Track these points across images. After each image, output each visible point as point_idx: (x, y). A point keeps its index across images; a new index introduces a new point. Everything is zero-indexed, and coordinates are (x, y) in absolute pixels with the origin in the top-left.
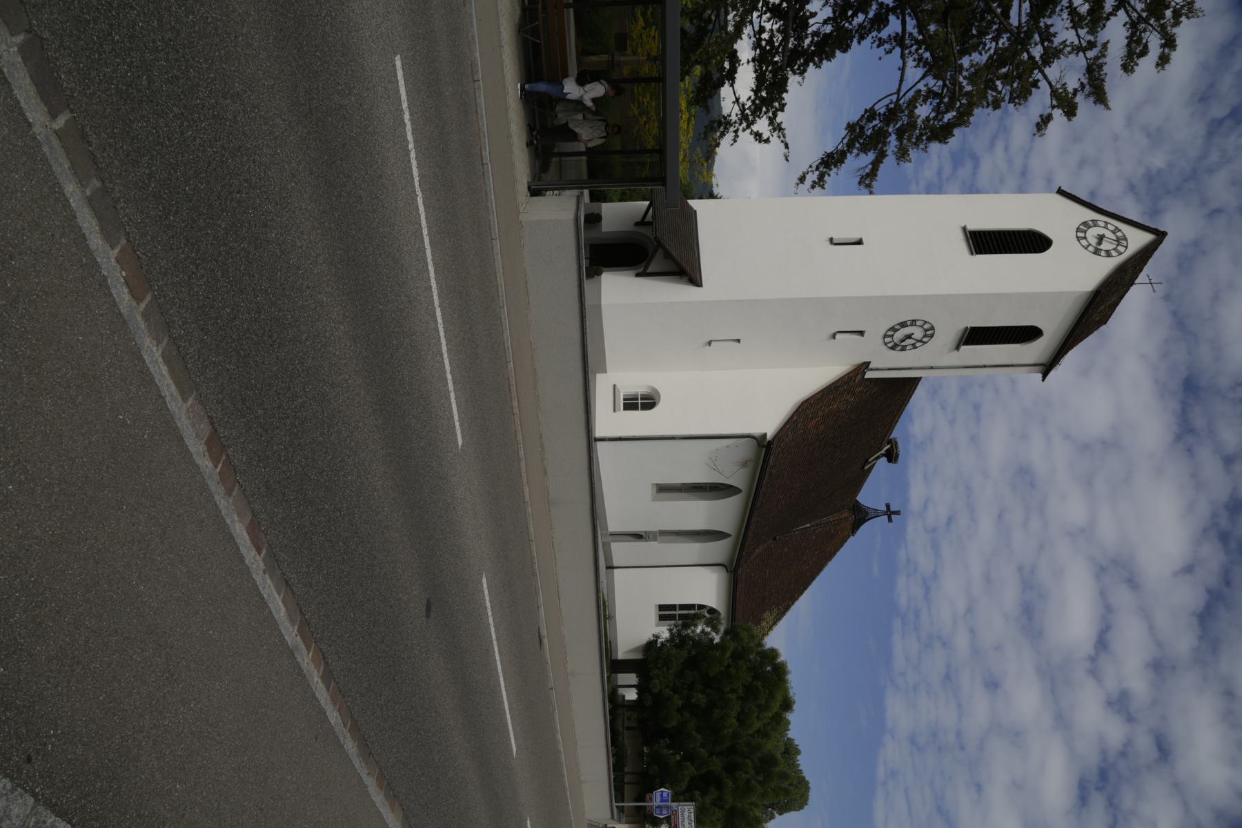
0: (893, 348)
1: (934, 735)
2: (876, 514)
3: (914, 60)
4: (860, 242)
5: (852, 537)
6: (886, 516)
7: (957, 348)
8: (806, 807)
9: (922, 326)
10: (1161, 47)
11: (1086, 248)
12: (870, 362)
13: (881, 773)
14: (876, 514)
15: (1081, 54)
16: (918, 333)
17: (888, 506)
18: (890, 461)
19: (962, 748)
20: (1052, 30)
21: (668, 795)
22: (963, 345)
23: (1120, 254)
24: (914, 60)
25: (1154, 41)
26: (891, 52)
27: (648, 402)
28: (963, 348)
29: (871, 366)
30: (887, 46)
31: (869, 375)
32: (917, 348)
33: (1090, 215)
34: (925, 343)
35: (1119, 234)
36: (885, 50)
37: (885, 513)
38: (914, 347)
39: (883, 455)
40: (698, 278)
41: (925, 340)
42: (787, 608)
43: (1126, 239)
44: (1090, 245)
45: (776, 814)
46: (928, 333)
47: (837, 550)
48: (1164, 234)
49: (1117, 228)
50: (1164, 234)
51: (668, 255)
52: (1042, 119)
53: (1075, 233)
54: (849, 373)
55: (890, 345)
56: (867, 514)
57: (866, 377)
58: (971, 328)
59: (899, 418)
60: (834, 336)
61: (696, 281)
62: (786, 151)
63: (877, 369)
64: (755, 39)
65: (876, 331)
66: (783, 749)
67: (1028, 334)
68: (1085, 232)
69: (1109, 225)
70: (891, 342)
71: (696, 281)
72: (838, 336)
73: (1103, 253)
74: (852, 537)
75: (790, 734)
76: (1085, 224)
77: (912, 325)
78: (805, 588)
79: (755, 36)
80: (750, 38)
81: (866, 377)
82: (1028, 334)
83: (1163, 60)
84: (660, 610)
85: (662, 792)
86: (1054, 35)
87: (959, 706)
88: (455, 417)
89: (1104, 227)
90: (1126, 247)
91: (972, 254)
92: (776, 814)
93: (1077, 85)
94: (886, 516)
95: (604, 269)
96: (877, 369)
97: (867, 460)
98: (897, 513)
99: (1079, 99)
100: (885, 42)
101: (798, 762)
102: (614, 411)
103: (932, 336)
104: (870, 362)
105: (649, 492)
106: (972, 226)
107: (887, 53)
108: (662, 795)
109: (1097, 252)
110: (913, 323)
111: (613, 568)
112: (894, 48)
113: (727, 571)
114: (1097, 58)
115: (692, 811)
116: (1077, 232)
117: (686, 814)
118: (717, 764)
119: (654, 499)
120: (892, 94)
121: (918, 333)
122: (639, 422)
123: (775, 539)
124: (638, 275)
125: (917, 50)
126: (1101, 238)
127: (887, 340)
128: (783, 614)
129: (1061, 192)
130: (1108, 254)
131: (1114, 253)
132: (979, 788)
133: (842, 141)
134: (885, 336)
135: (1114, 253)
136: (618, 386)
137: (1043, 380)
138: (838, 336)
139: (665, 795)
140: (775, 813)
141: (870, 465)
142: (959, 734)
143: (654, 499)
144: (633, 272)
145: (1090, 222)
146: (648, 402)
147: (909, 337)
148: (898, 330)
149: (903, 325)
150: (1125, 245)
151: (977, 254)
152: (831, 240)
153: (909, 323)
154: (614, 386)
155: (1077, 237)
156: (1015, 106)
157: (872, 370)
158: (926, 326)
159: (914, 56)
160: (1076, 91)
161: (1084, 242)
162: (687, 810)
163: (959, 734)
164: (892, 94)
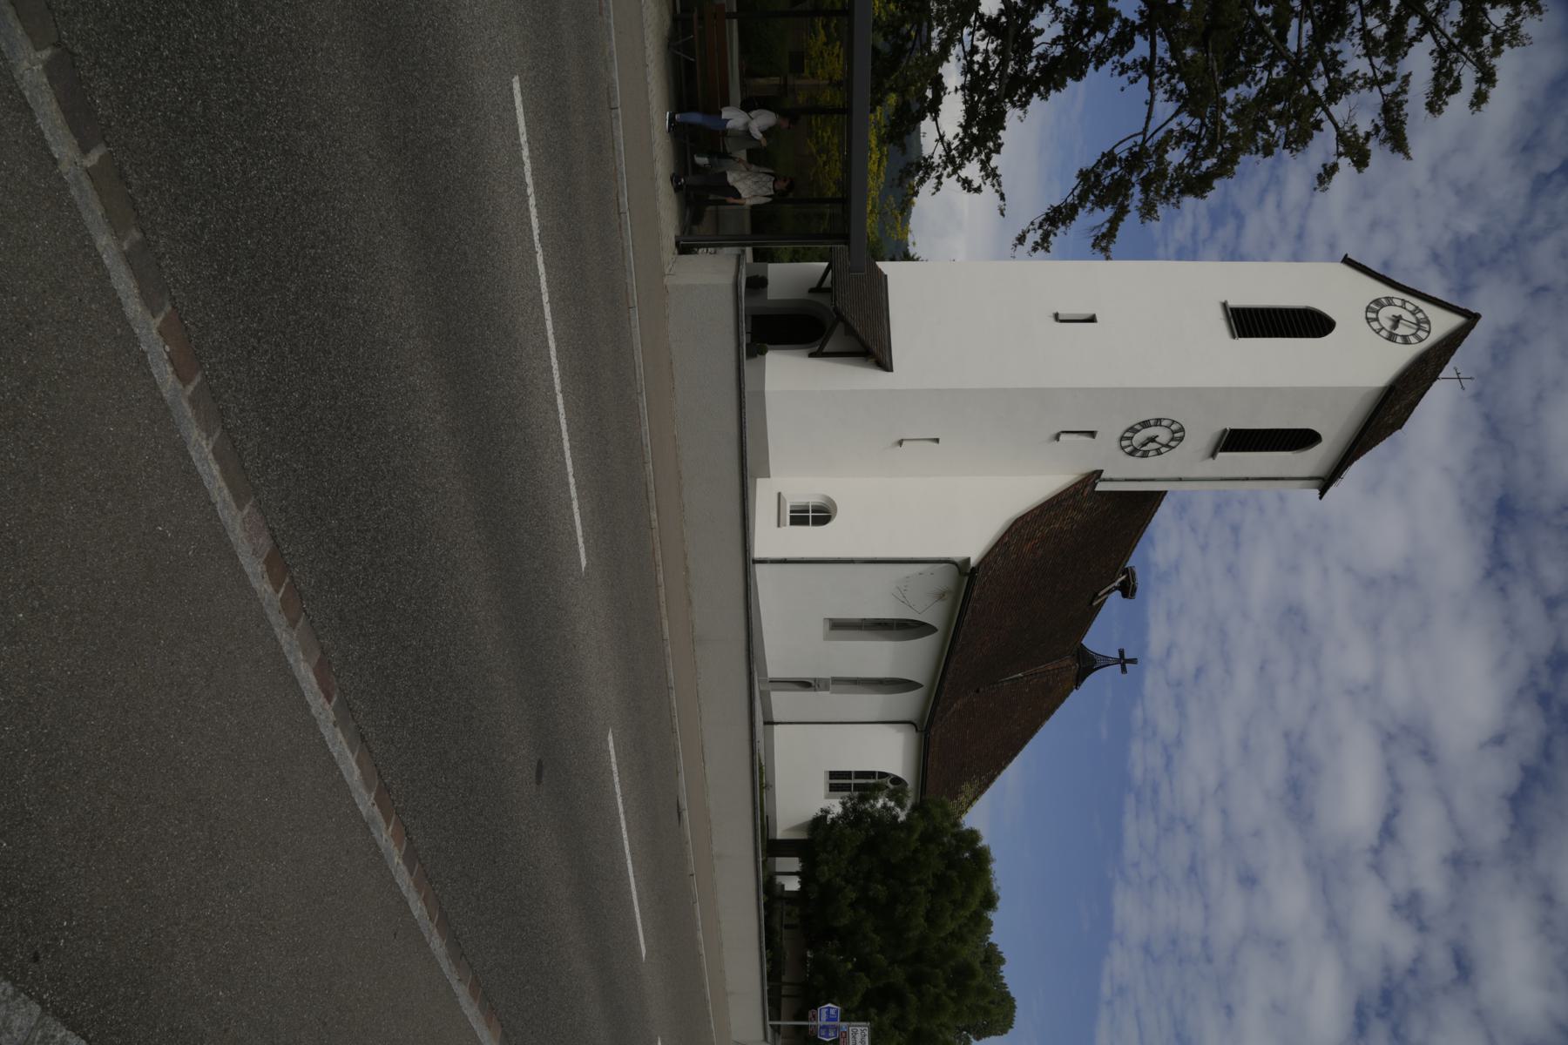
0: (1131, 454)
1: (1174, 942)
2: (1107, 662)
3: (1166, 92)
4: (1092, 319)
5: (1075, 690)
7: (1213, 455)
8: (1010, 1031)
10: (1477, 82)
11: (1378, 333)
12: (1102, 471)
13: (1106, 989)
14: (1107, 662)
15: (1376, 89)
16: (1163, 435)
17: (1121, 652)
18: (1125, 595)
19: (1209, 960)
20: (1340, 58)
21: (836, 1012)
22: (1221, 451)
23: (1421, 340)
24: (1166, 92)
25: (1468, 75)
26: (1136, 82)
27: (820, 515)
28: (1220, 455)
29: (1103, 476)
30: (1131, 74)
31: (1101, 487)
33: (1383, 291)
35: (1420, 316)
36: (1129, 78)
37: (1117, 661)
38: (1159, 453)
39: (1116, 588)
40: (888, 360)
41: (1173, 444)
42: (992, 779)
43: (1428, 322)
44: (1383, 328)
45: (972, 1040)
46: (1176, 435)
47: (1057, 706)
48: (1476, 317)
49: (1417, 308)
50: (1476, 317)
51: (850, 331)
52: (1325, 169)
54: (1076, 484)
55: (1128, 450)
57: (1097, 489)
58: (1231, 430)
60: (1057, 437)
61: (884, 364)
62: (1002, 203)
63: (1111, 480)
64: (965, 62)
65: (1110, 430)
66: (983, 958)
67: (1302, 439)
68: (1377, 312)
69: (1407, 304)
71: (884, 364)
72: (1063, 437)
73: (1399, 339)
74: (1075, 690)
75: (992, 938)
76: (1377, 301)
77: (1156, 425)
79: (965, 58)
80: (959, 60)
81: (1097, 489)
82: (1302, 439)
83: (1479, 99)
85: (829, 1008)
86: (1343, 64)
87: (1206, 907)
89: (1401, 307)
90: (1429, 332)
91: (1234, 337)
92: (972, 1040)
93: (1370, 128)
95: (768, 346)
96: (1111, 480)
97: (1097, 594)
98: (1133, 661)
99: (1372, 145)
100: (1129, 68)
101: (1001, 974)
102: (779, 526)
103: (1181, 439)
104: (1102, 471)
105: (820, 628)
106: (1233, 303)
107: (1131, 82)
108: (828, 1013)
109: (1391, 338)
110: (1158, 422)
111: (773, 723)
112: (1140, 77)
113: (917, 730)
114: (1396, 94)
115: (867, 1033)
116: (1367, 312)
117: (859, 1037)
118: (898, 975)
119: (827, 638)
120: (1136, 135)
121: (1163, 435)
122: (809, 541)
123: (978, 691)
124: (811, 355)
125: (1169, 80)
126: (1397, 320)
127: (1125, 443)
128: (987, 786)
129: (1347, 261)
130: (1406, 341)
131: (1413, 339)
132: (1229, 1010)
133: (1072, 192)
134: (1122, 438)
135: (1413, 339)
136: (783, 494)
137: (1321, 498)
138: (1063, 437)
139: (832, 1012)
140: (971, 1037)
141: (1099, 601)
142: (1205, 942)
143: (827, 638)
144: (805, 352)
145: (1383, 300)
146: (820, 515)
148: (1139, 431)
149: (1145, 424)
150: (1427, 329)
151: (1240, 337)
152: (1056, 316)
153: (1152, 422)
154: (779, 494)
155: (1367, 318)
156: (1291, 152)
157: (1104, 480)
158: (1174, 427)
159: (1165, 87)
160: (1368, 135)
161: (1375, 325)
162: (859, 1032)
163: (1205, 942)
164: (1136, 135)
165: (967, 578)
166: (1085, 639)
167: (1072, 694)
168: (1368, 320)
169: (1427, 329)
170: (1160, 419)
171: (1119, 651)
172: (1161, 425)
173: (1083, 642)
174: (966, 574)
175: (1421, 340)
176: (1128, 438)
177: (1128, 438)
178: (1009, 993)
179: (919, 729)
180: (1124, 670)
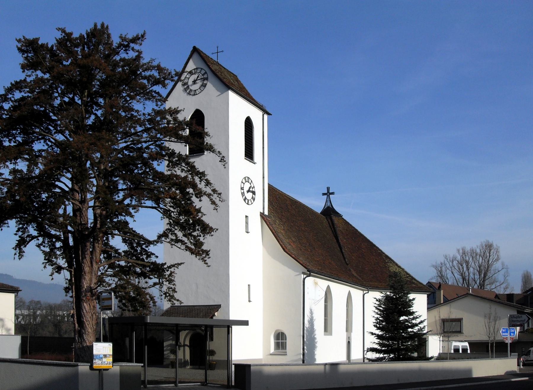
2: (329, 200)
5: (343, 217)
6: (327, 192)
9: (244, 184)
12: (260, 212)
14: (329, 200)
16: (247, 186)
17: (324, 194)
21: (504, 329)
29: (262, 212)
31: (266, 213)
32: (254, 186)
34: (252, 181)
37: (328, 197)
41: (250, 181)
42: (387, 257)
48: (194, 48)
50: (194, 48)
53: (191, 96)
55: (252, 201)
56: (328, 207)
57: (267, 214)
58: (245, 156)
59: (280, 191)
63: (264, 208)
70: (251, 201)
74: (343, 217)
76: (185, 90)
77: (243, 190)
78: (374, 246)
81: (267, 214)
84: (286, 352)
85: (502, 332)
88: (441, 386)
89: (189, 79)
90: (202, 69)
94: (327, 192)
96: (264, 208)
98: (328, 189)
103: (249, 178)
104: (260, 212)
108: (504, 332)
110: (242, 189)
127: (250, 203)
128: (390, 259)
137: (271, 115)
139: (504, 331)
147: (25, 93)
148: (245, 197)
150: (200, 69)
158: (244, 181)
162: (512, 319)
165: (312, 274)
166: (318, 212)
167: (345, 218)
168: (189, 94)
169: (200, 69)
170: (241, 188)
171: (323, 195)
172: (243, 188)
173: (319, 213)
174: (310, 274)
175: (206, 73)
176: (248, 202)
177: (248, 202)
178: (76, 37)
179: (367, 292)
180: (333, 193)
